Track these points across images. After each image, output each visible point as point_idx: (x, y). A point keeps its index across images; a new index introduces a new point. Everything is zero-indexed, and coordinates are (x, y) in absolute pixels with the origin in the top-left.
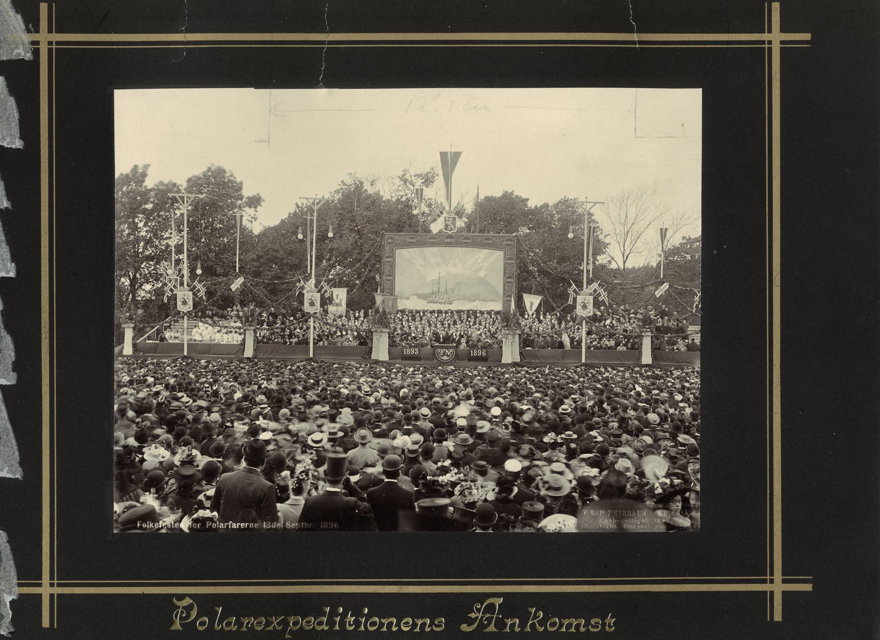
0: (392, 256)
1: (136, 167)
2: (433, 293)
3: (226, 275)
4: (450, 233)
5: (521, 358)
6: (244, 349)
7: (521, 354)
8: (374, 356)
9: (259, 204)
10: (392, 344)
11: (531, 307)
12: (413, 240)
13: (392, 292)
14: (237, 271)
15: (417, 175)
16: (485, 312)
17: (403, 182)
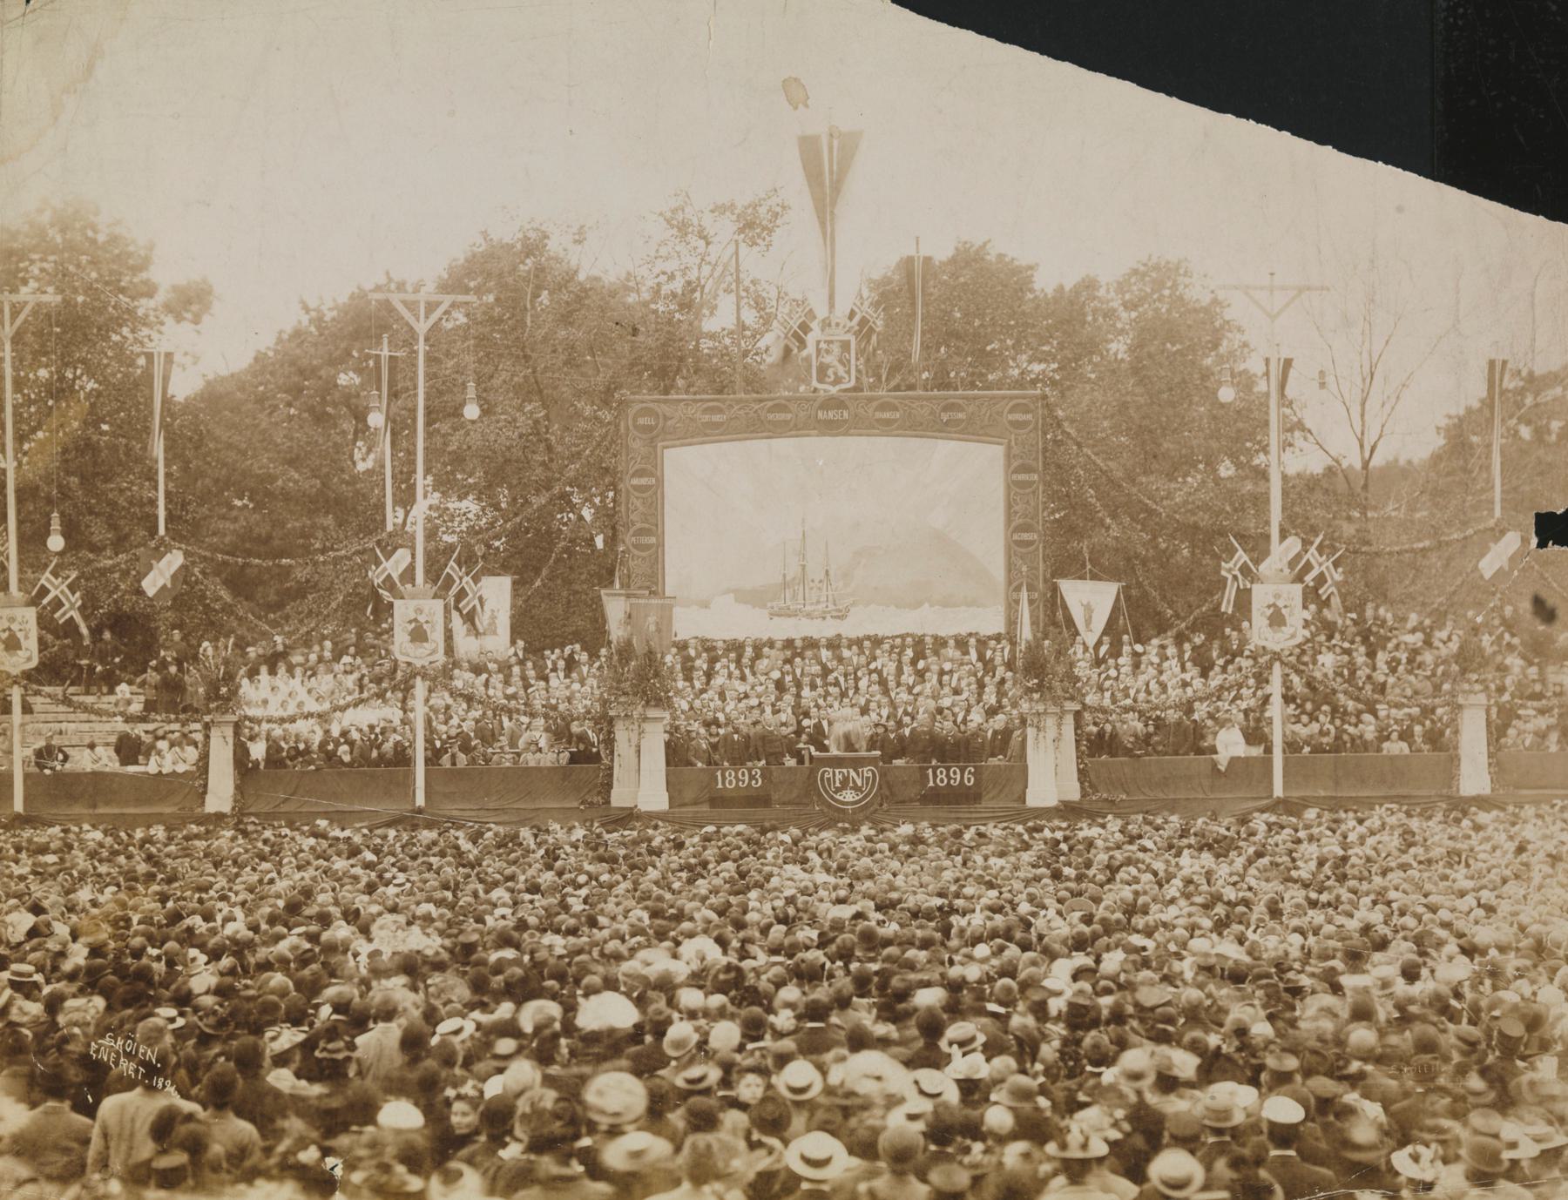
0: (652, 469)
1: (281, 332)
2: (785, 585)
3: (120, 543)
4: (834, 390)
5: (1082, 788)
6: (205, 786)
7: (1083, 774)
8: (620, 797)
9: (206, 307)
10: (677, 753)
11: (1088, 622)
12: (717, 418)
13: (653, 583)
14: (162, 531)
15: (719, 209)
16: (952, 643)
17: (675, 231)
